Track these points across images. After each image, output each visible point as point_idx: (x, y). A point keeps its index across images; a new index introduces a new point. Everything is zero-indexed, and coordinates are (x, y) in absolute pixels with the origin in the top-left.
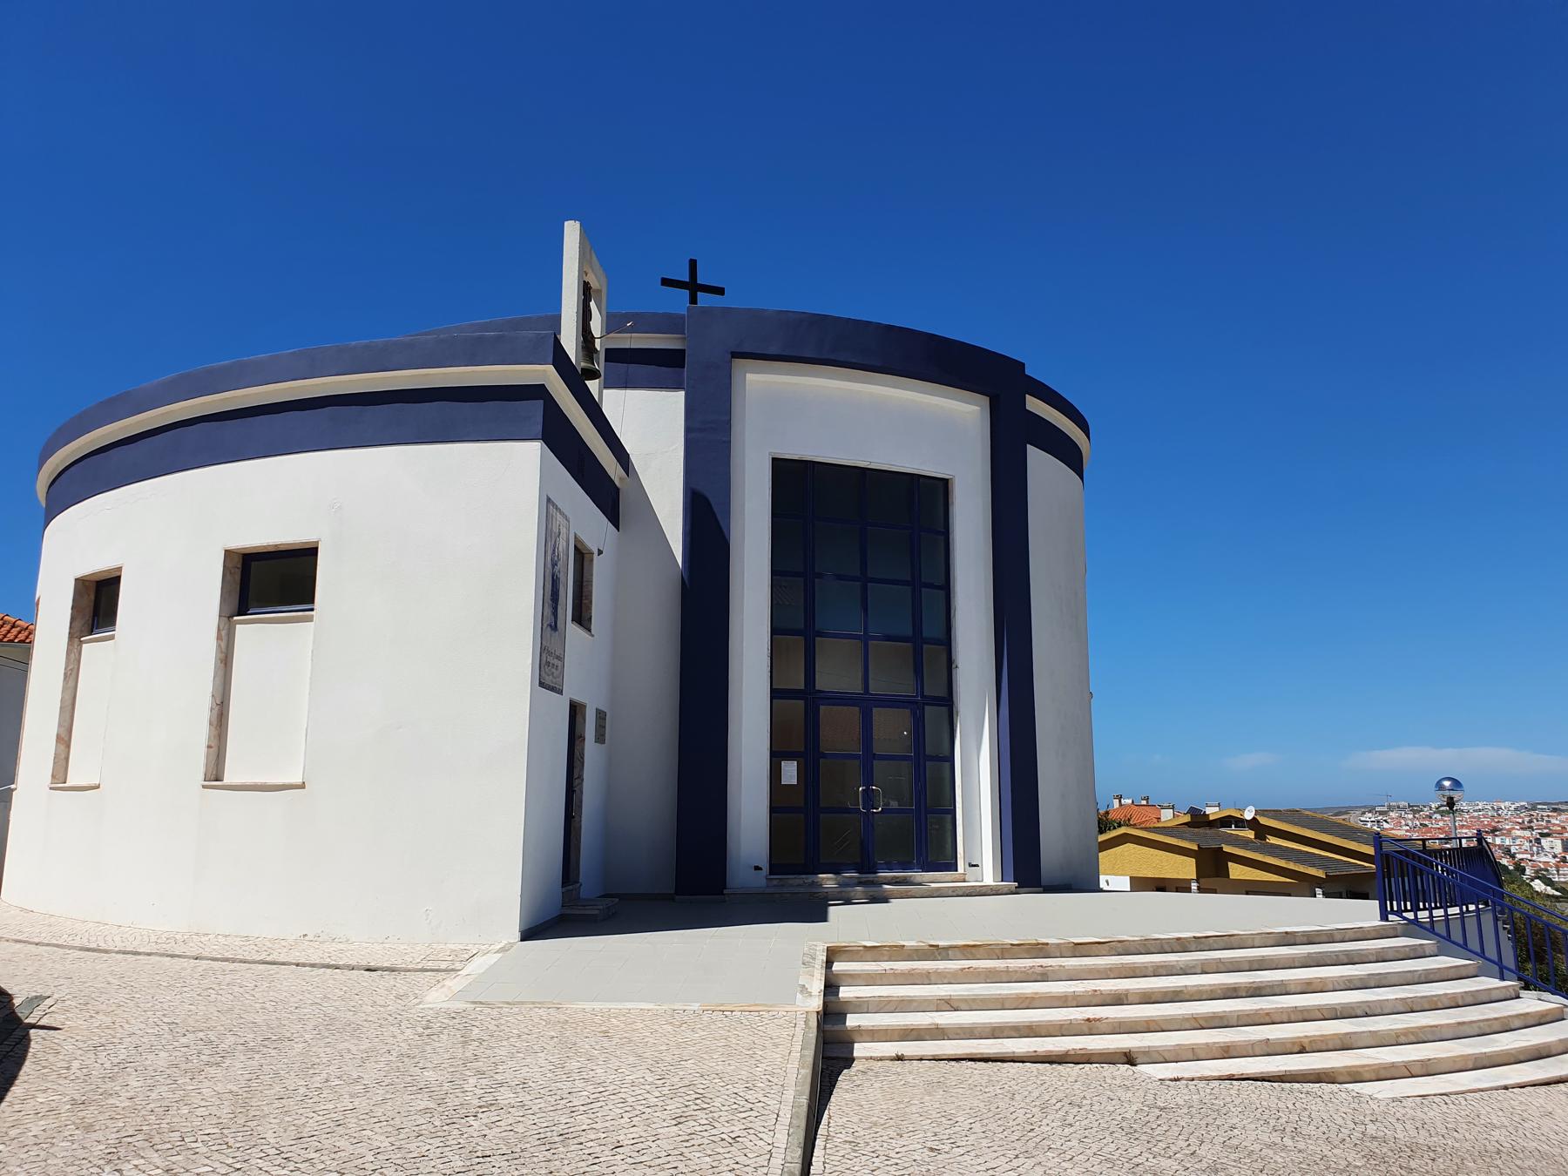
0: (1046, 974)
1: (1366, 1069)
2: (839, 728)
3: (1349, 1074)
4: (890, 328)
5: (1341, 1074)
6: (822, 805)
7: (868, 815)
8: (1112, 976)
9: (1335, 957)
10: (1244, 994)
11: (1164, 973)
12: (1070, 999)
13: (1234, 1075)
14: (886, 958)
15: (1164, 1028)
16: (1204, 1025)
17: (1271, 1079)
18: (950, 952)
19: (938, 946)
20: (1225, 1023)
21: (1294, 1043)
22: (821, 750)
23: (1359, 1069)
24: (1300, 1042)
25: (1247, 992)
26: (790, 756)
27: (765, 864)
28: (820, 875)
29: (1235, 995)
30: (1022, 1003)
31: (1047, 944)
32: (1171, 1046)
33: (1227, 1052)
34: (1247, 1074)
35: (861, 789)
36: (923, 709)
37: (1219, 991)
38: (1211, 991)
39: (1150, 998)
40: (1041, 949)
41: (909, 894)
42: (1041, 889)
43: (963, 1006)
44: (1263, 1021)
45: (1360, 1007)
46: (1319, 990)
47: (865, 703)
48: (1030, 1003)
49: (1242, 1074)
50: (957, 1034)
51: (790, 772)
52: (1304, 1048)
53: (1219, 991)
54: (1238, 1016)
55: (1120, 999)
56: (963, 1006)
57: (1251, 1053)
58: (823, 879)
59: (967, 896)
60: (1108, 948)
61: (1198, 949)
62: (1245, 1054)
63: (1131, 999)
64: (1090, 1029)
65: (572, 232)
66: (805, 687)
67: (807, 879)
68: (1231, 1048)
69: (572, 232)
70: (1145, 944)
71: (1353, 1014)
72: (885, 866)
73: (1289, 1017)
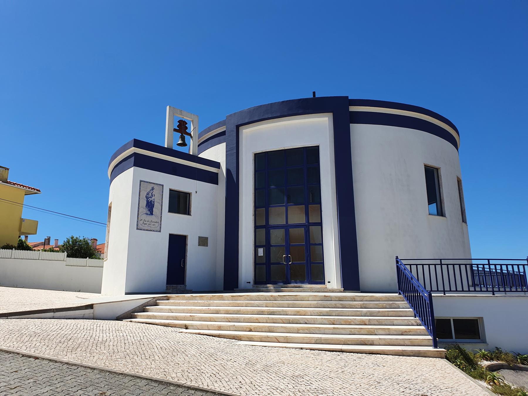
0: (210, 304)
1: (256, 337)
2: (277, 236)
3: (247, 338)
4: (283, 102)
5: (244, 337)
6: (272, 262)
7: (288, 264)
8: (230, 306)
9: (334, 305)
10: (266, 314)
11: (250, 306)
12: (202, 311)
13: (200, 333)
14: (181, 300)
15: (216, 321)
16: (230, 321)
17: (215, 336)
18: (197, 298)
19: (193, 296)
20: (239, 321)
21: (247, 328)
22: (271, 244)
23: (253, 337)
24: (250, 327)
25: (267, 313)
26: (260, 247)
27: (252, 282)
28: (268, 285)
29: (262, 314)
30: (189, 311)
31: (223, 296)
32: (199, 324)
33: (220, 328)
34: (205, 333)
35: (284, 256)
36: (309, 227)
37: (256, 312)
38: (252, 311)
39: (229, 312)
40: (222, 298)
41: (292, 291)
42: (360, 291)
43: (174, 312)
44: (255, 321)
45: (303, 320)
46: (303, 315)
47: (287, 227)
48: (191, 311)
49: (203, 333)
50: (159, 318)
51: (261, 252)
52: (251, 330)
53: (256, 312)
54: (244, 319)
55: (218, 312)
56: (174, 312)
57: (229, 329)
58: (269, 286)
59: (317, 292)
60: (244, 298)
61: (282, 300)
62: (226, 330)
63: (221, 312)
64: (192, 319)
65: (168, 107)
66: (266, 224)
67: (264, 286)
68: (222, 327)
69: (168, 107)
70: (259, 297)
71: (299, 322)
72: (294, 282)
73: (267, 321)
